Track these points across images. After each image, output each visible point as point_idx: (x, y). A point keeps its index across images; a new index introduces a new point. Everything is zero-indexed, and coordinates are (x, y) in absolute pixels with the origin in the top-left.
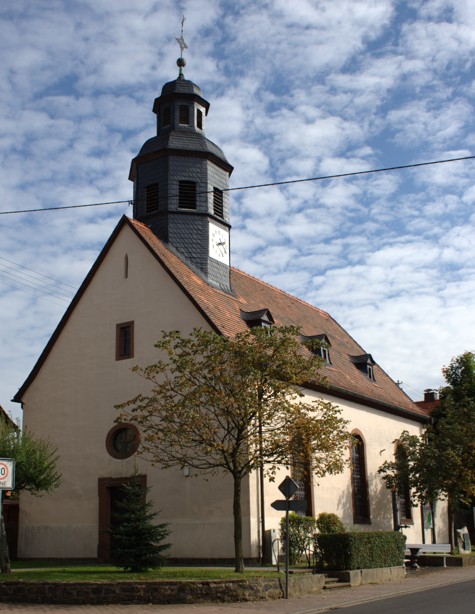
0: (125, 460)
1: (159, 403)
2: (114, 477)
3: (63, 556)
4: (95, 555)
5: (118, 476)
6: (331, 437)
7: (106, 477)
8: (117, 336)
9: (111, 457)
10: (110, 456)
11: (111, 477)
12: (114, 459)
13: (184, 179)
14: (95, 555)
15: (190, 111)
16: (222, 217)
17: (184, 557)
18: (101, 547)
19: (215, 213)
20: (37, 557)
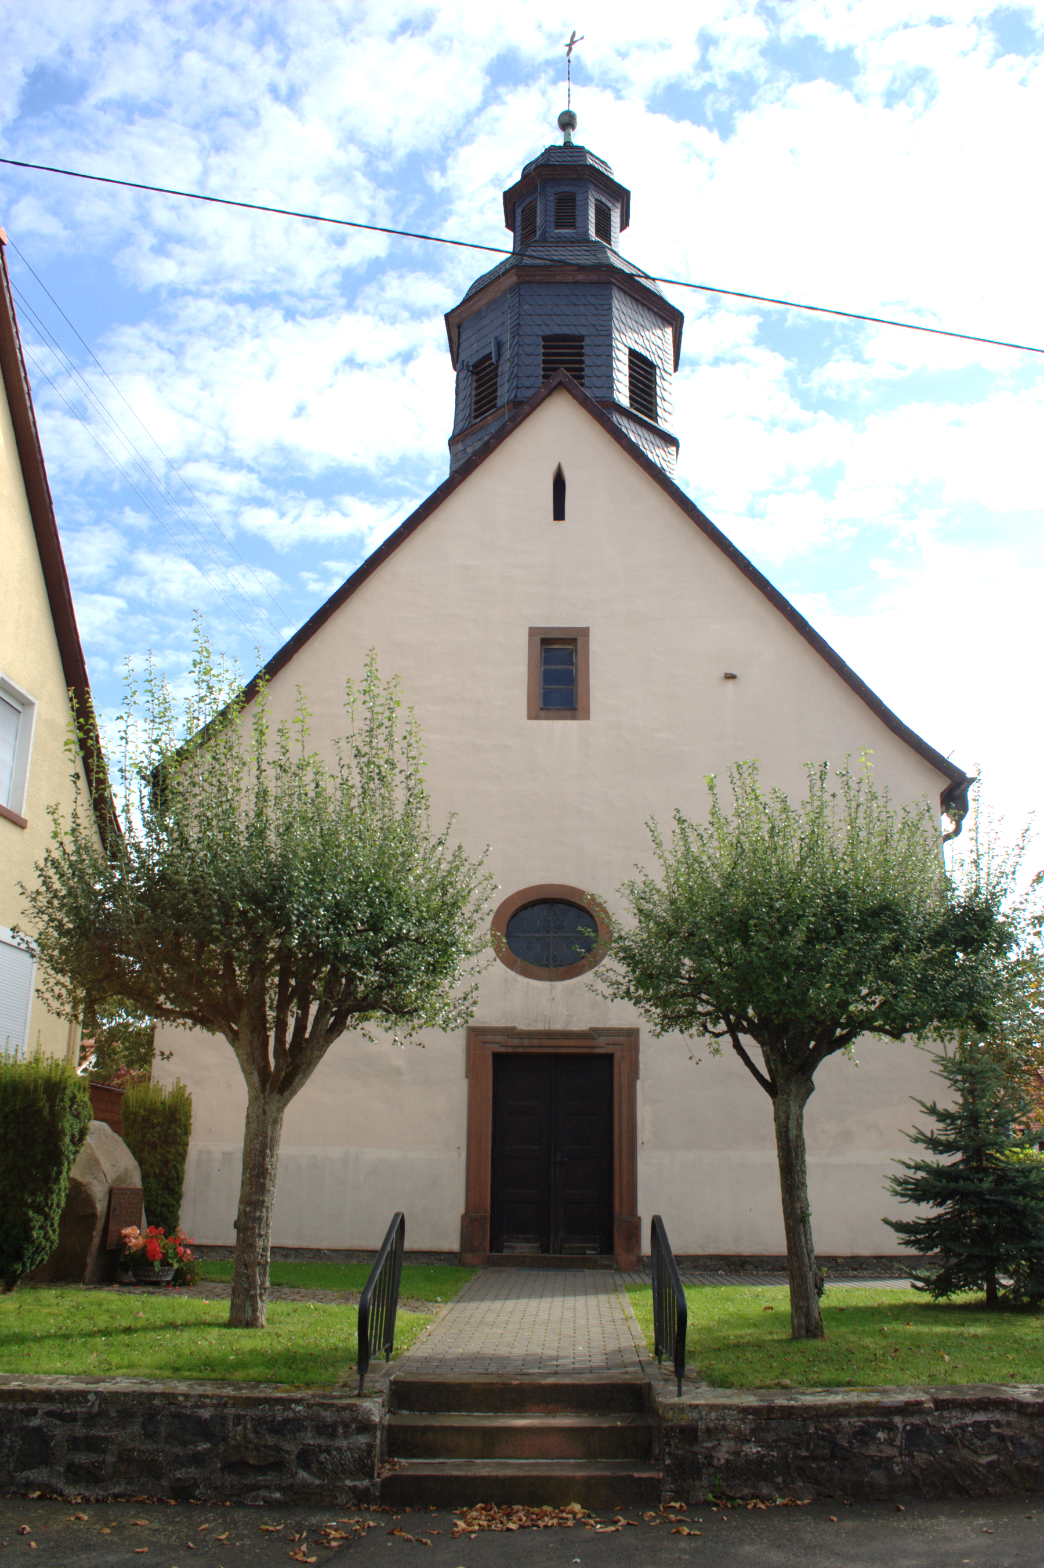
0: (560, 985)
1: (1038, 929)
2: (522, 1026)
3: (325, 1244)
4: (452, 1243)
5: (540, 1027)
6: (243, 982)
7: (494, 1024)
8: (529, 697)
9: (512, 973)
10: (509, 970)
11: (514, 1028)
12: (520, 978)
13: (557, 331)
14: (452, 1243)
15: (578, 219)
16: (654, 416)
17: (765, 1253)
18: (469, 1222)
19: (631, 405)
20: (219, 1243)
